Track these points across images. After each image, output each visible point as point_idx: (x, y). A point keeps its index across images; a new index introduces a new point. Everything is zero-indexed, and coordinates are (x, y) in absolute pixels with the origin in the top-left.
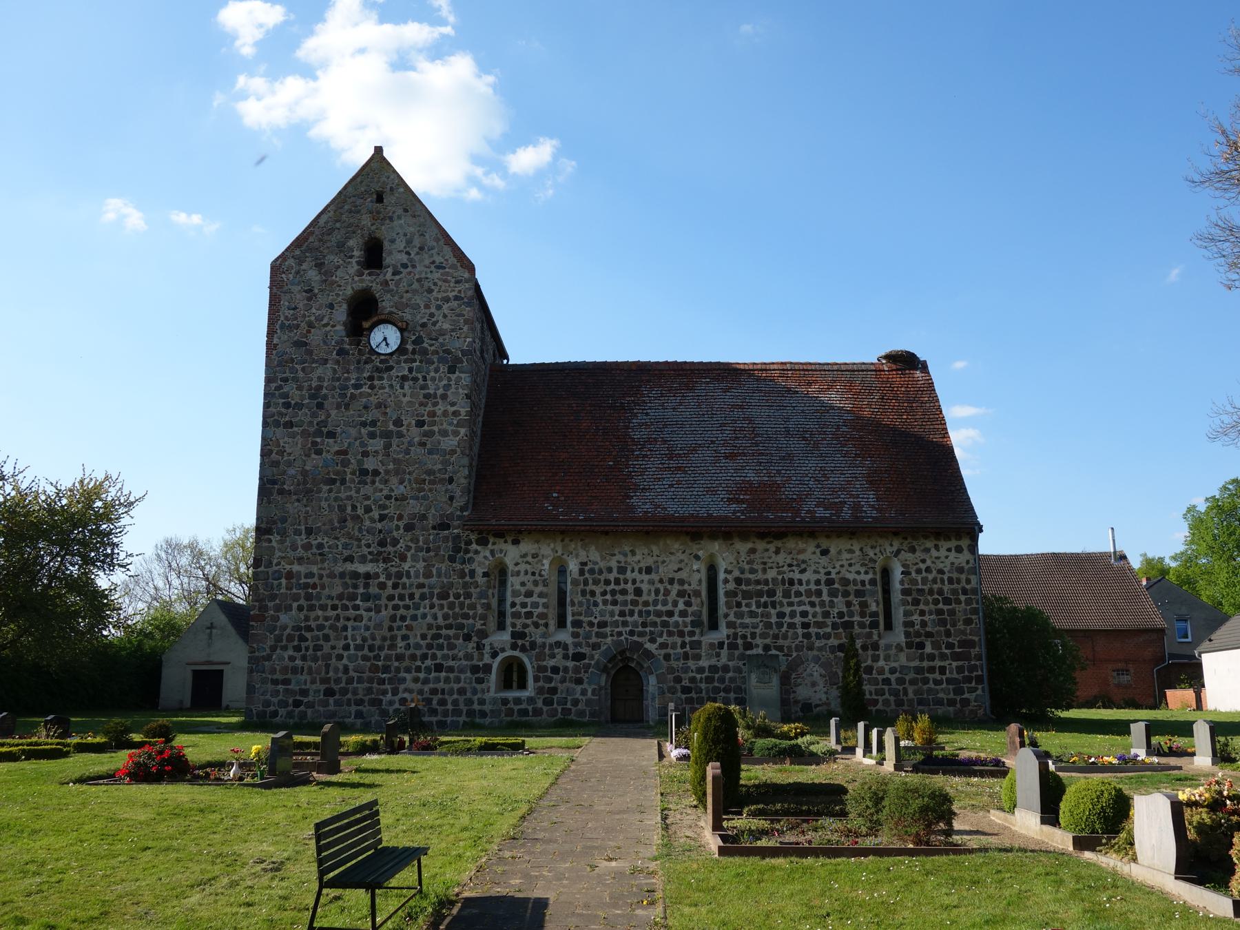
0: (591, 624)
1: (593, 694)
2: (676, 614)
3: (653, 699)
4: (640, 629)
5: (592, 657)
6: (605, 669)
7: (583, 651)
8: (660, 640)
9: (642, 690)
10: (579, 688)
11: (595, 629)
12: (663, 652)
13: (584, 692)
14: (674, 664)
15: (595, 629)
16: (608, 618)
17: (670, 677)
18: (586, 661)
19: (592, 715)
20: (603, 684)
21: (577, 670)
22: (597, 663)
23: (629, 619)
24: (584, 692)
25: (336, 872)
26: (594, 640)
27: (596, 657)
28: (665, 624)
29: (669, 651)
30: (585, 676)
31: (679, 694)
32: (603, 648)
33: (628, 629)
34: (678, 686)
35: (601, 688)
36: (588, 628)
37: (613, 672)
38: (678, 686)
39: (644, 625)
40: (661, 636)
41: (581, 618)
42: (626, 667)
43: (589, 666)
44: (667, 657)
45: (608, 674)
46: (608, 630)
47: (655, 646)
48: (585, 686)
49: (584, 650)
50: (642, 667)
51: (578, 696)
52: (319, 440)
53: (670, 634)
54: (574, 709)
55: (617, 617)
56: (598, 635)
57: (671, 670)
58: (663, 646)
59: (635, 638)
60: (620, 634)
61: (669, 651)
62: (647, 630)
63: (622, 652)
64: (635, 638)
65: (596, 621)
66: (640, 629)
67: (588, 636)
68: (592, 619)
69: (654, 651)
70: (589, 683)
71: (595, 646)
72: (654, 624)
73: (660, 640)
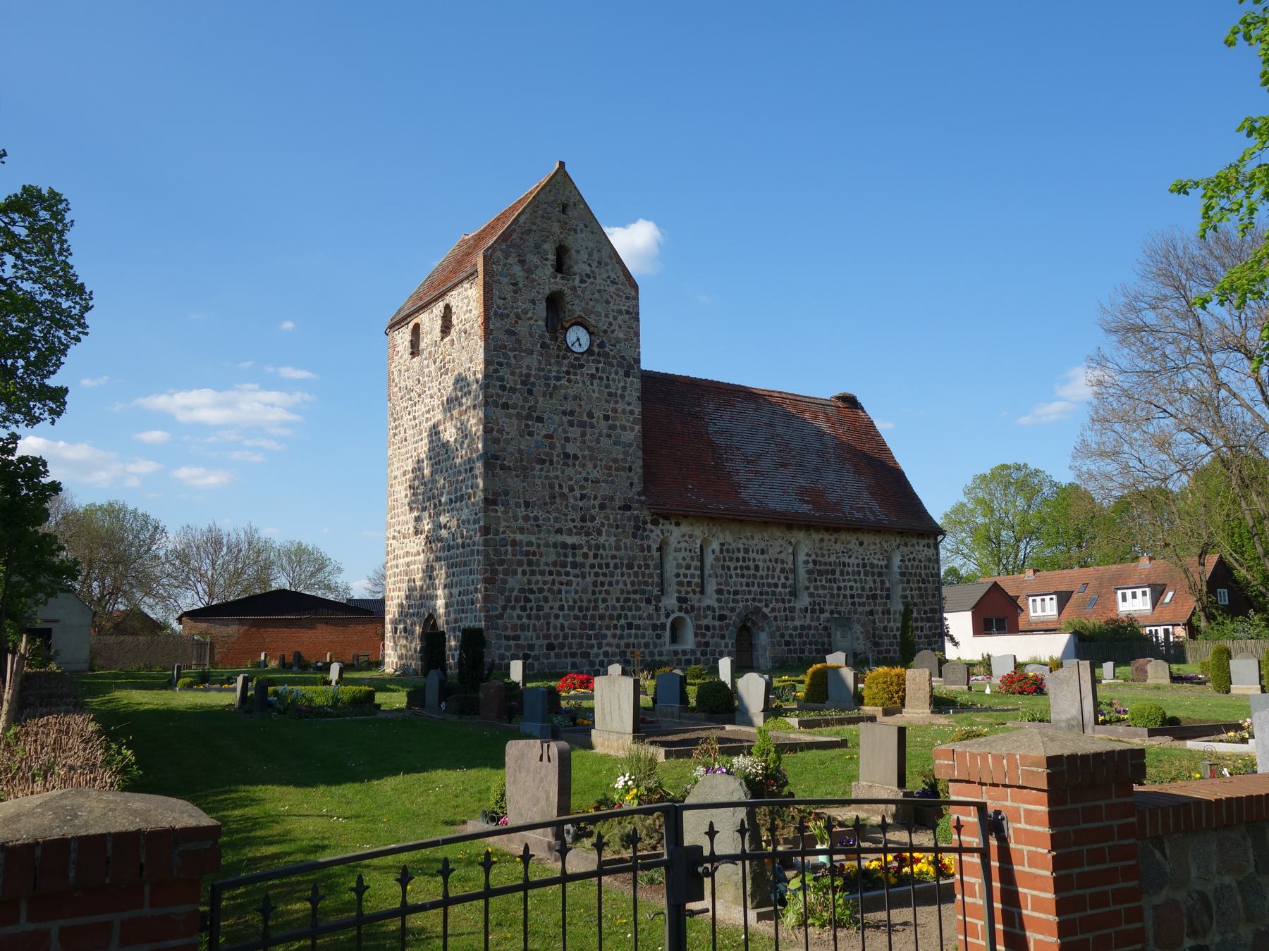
10: (723, 642)
16: (739, 588)
26: (731, 605)
39: (761, 594)
46: (739, 597)
53: (777, 601)
58: (773, 610)
60: (747, 600)
71: (733, 609)
72: (767, 593)
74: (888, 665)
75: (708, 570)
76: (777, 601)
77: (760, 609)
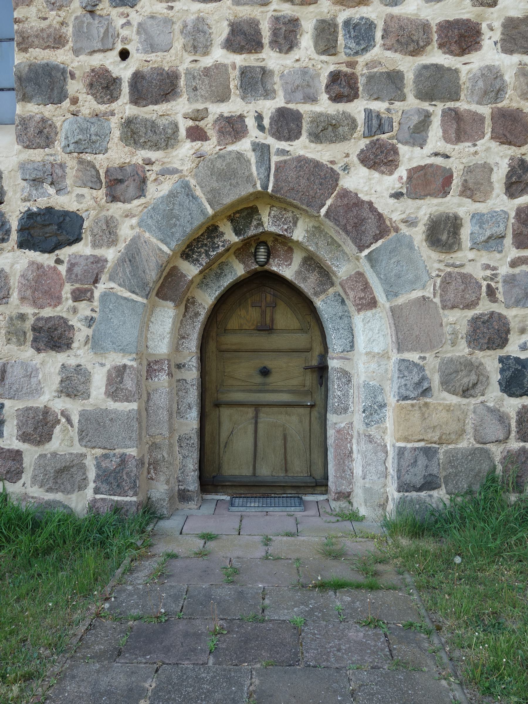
0: (104, 85)
1: (115, 390)
2: (490, 38)
3: (374, 410)
4: (325, 106)
5: (108, 232)
6: (168, 286)
7: (66, 202)
8: (411, 157)
9: (322, 371)
10: (51, 365)
11: (124, 107)
12: (427, 208)
13: (73, 384)
14: (472, 261)
15: (124, 107)
16: (177, 59)
17: (458, 320)
18: (83, 249)
19: (110, 479)
20: (161, 347)
21: (41, 288)
22: (132, 256)
23: (271, 59)
24: (73, 384)
25: (272, 178)
26: (117, 154)
27: (126, 231)
28: (438, 85)
29: (454, 204)
30: (78, 317)
31: (493, 395)
32: (158, 190)
33: (268, 107)
34: (490, 362)
35: (152, 368)
36: (89, 104)
37: (207, 299)
38: (490, 362)
39: (343, 87)
40: (418, 133)
41: (61, 57)
42: (264, 280)
43: (94, 271)
44: (443, 233)
45: (188, 305)
46: (178, 110)
47: (395, 180)
48: (79, 355)
49: (74, 199)
50: (326, 276)
51: (48, 398)
52: (173, 230)
53: (461, 127)
54: (31, 454)
55: (219, 55)
56: (132, 133)
57: (459, 289)
58: (429, 181)
59: (302, 147)
60: (233, 128)
61: (454, 204)
62: (357, 109)
63: (243, 213)
64: (302, 147)
65: (124, 72)
66: (325, 106)
67: (88, 142)
68: (110, 61)
69: (387, 206)
70: (95, 344)
71: (119, 184)
72: (390, 83)
73: (411, 157)
74: (380, 239)
75: (437, 288)
76: (461, 127)
77: (325, 177)
